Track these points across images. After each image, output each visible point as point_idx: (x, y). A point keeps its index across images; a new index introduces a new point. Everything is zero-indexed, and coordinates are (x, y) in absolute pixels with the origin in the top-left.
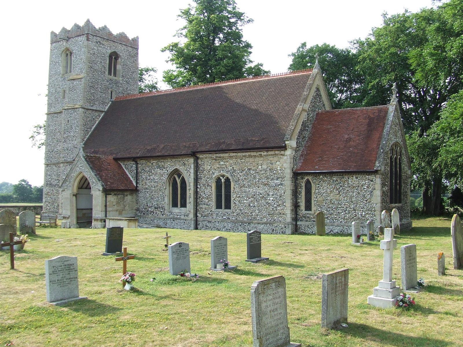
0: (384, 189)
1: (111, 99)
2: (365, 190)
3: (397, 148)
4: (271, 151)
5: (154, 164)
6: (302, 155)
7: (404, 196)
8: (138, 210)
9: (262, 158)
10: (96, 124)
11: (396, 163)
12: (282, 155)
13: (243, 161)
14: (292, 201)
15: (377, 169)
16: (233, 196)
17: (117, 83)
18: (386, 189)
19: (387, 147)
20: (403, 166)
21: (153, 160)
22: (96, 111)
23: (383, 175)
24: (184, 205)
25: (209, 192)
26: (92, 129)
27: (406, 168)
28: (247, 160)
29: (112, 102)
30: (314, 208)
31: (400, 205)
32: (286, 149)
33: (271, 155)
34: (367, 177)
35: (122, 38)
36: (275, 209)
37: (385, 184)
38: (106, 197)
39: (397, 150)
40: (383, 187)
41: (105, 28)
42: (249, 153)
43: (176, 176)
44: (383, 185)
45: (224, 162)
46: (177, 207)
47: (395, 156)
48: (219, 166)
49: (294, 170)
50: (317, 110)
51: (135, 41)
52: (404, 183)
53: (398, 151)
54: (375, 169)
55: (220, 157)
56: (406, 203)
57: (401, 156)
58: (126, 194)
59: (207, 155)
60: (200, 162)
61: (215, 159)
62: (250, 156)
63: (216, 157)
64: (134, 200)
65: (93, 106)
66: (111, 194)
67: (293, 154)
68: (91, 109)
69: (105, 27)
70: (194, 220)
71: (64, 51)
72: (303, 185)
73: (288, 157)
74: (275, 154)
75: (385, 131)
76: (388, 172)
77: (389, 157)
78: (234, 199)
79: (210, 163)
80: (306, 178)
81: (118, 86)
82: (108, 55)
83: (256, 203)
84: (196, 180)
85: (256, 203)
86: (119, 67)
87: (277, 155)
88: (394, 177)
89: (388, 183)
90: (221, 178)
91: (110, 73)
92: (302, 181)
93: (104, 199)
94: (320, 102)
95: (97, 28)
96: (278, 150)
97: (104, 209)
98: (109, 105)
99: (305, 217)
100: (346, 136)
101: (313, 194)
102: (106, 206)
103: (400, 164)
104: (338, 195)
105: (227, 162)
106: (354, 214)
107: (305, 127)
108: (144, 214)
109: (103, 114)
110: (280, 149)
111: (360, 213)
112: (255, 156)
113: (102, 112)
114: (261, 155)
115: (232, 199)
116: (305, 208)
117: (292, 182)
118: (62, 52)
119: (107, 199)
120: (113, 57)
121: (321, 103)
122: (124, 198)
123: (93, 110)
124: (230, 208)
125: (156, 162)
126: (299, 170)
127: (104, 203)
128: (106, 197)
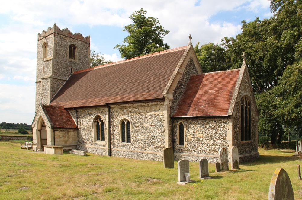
0: (236, 129)
1: (71, 72)
2: (221, 130)
3: (247, 100)
4: (154, 102)
5: (86, 112)
6: (178, 105)
7: (253, 135)
8: (78, 141)
9: (149, 108)
10: (61, 88)
11: (246, 111)
12: (162, 104)
13: (137, 109)
14: (169, 138)
15: (230, 114)
16: (132, 134)
17: (75, 63)
18: (237, 129)
19: (238, 99)
20: (252, 113)
21: (86, 109)
22: (61, 80)
23: (235, 119)
24: (103, 139)
25: (117, 130)
26: (58, 91)
27: (255, 115)
28: (140, 108)
29: (72, 75)
30: (185, 143)
31: (250, 141)
32: (165, 100)
33: (155, 105)
34: (223, 120)
35: (79, 36)
36: (158, 143)
37: (237, 126)
38: (54, 132)
39: (247, 102)
40: (235, 128)
41: (66, 30)
42: (141, 104)
43: (99, 120)
44: (234, 127)
45: (126, 110)
46: (125, 142)
47: (246, 105)
48: (123, 113)
49: (171, 115)
50: (191, 74)
51: (88, 38)
52: (253, 126)
53: (248, 102)
54: (228, 114)
55: (123, 107)
56: (255, 140)
57: (250, 106)
58: (69, 130)
59: (116, 106)
60: (111, 110)
61: (121, 109)
62: (142, 106)
63: (121, 107)
64: (76, 135)
65: (58, 77)
66: (58, 131)
67: (171, 104)
68: (57, 79)
69: (67, 29)
70: (109, 149)
71: (43, 44)
72: (178, 126)
73: (166, 106)
74: (158, 104)
75: (236, 86)
76: (239, 117)
77: (241, 106)
78: (132, 136)
79: (118, 111)
80: (180, 121)
81: (76, 65)
82: (68, 46)
83: (146, 139)
84: (110, 122)
85: (146, 139)
86: (76, 54)
87: (159, 105)
88: (244, 121)
89: (239, 125)
90: (124, 121)
91: (70, 57)
92: (177, 123)
93: (53, 133)
94: (194, 69)
95: (61, 29)
96: (159, 101)
97: (53, 140)
98: (69, 77)
99: (179, 150)
100: (209, 91)
101: (184, 133)
102: (54, 138)
103: (250, 112)
104: (202, 134)
105: (128, 110)
106: (214, 148)
107: (181, 85)
108: (82, 144)
109: (65, 82)
110: (160, 100)
111: (217, 148)
112: (145, 106)
113: (65, 81)
114: (148, 105)
115: (131, 136)
116: (180, 143)
117: (170, 125)
118: (43, 45)
119: (55, 133)
120: (73, 48)
121: (195, 69)
122: (68, 133)
123: (58, 79)
124: (130, 142)
125: (87, 110)
126: (175, 116)
127: (53, 136)
128: (54, 132)
